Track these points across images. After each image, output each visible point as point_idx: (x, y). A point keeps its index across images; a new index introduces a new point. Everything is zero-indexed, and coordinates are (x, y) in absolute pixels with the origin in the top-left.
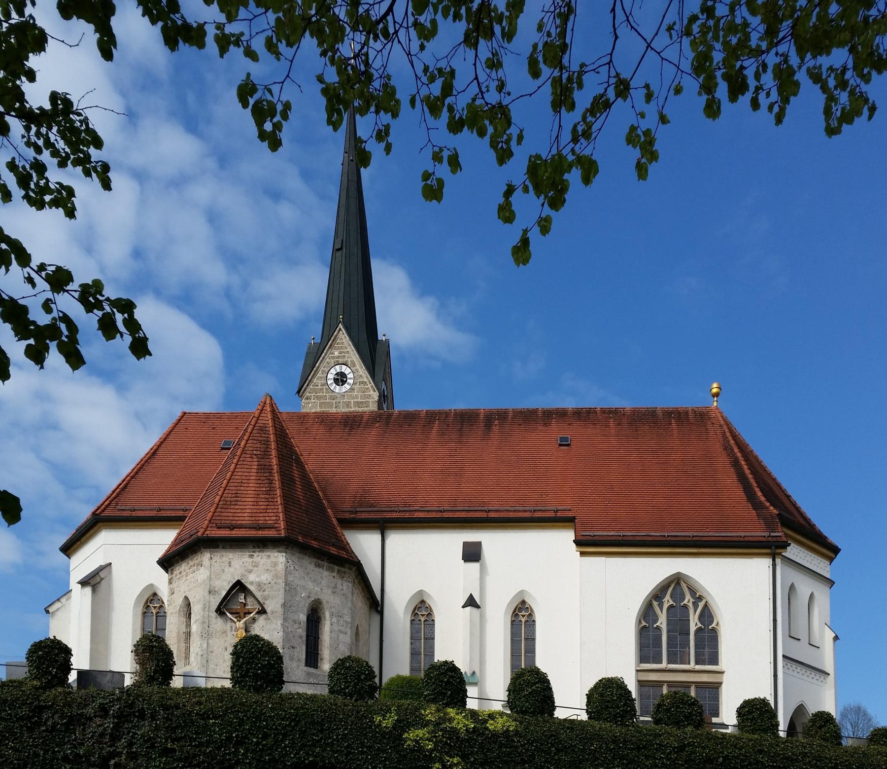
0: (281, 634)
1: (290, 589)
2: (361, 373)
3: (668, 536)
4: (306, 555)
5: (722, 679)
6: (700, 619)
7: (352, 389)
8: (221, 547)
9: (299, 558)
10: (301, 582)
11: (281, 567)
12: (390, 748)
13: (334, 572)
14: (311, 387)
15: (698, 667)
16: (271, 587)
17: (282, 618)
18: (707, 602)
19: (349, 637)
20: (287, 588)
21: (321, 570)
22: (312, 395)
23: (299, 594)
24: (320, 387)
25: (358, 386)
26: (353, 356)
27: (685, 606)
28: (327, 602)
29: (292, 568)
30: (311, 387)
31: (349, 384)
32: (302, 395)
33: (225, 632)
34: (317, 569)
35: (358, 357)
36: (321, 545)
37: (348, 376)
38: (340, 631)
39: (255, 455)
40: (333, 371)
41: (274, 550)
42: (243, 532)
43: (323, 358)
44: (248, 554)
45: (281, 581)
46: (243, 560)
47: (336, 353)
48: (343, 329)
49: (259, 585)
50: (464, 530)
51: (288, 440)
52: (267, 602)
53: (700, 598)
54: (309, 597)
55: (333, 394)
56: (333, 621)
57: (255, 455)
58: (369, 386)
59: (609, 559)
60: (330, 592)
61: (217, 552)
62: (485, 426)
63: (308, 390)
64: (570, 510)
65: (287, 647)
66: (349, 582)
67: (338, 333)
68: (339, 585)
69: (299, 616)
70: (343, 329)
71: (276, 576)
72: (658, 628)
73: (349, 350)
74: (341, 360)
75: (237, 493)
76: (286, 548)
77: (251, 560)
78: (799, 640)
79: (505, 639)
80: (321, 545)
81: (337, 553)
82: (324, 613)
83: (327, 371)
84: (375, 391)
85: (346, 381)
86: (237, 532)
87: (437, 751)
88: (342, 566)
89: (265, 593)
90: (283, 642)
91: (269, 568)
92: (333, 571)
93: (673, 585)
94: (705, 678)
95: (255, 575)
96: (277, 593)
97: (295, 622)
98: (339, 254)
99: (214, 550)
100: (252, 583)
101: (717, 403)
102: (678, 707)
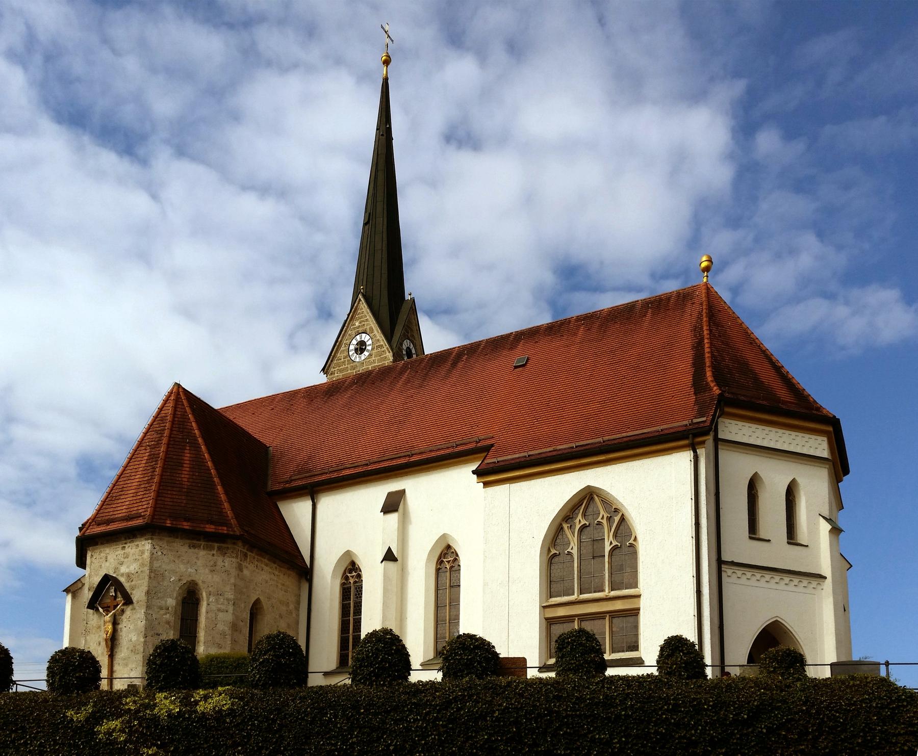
0: (144, 622)
1: (155, 575)
2: (378, 338)
3: (576, 447)
4: (177, 538)
5: (639, 604)
6: (615, 536)
7: (370, 355)
8: (99, 543)
9: (168, 542)
10: (172, 566)
11: (147, 555)
12: (82, 743)
13: (214, 550)
14: (335, 362)
15: (614, 593)
16: (138, 577)
17: (145, 607)
18: (623, 514)
19: (231, 615)
20: (153, 575)
21: (196, 550)
22: (336, 369)
23: (168, 579)
24: (342, 360)
25: (376, 351)
26: (372, 323)
27: (599, 524)
28: (203, 582)
29: (160, 553)
30: (335, 362)
31: (368, 351)
32: (327, 372)
33: (99, 627)
34: (192, 550)
35: (375, 322)
36: (195, 525)
37: (367, 343)
38: (219, 610)
39: (149, 446)
40: (354, 342)
41: (142, 539)
42: (116, 526)
43: (346, 331)
44: (121, 546)
45: (146, 569)
46: (117, 553)
47: (357, 324)
48: (362, 299)
49: (129, 576)
50: (372, 483)
51: (189, 424)
52: (134, 592)
53: (616, 511)
54: (180, 580)
55: (355, 364)
56: (211, 600)
57: (149, 446)
58: (385, 348)
59: (513, 485)
60: (207, 571)
61: (97, 549)
62: (452, 364)
63: (333, 365)
64: (493, 437)
65: (150, 634)
66: (233, 557)
67: (359, 303)
68: (220, 563)
69: (166, 601)
70: (362, 299)
71: (143, 565)
72: (569, 553)
73: (368, 317)
74: (361, 330)
75: (123, 488)
76: (152, 535)
77: (123, 552)
78: (769, 541)
79: (427, 591)
80: (195, 525)
81: (213, 530)
82: (202, 594)
83: (349, 343)
84: (389, 352)
85: (365, 348)
86: (112, 527)
87: (131, 743)
88: (224, 542)
89: (133, 583)
90: (145, 630)
91: (137, 557)
92: (212, 548)
93: (585, 503)
94: (619, 605)
95: (125, 567)
96: (143, 581)
97: (161, 608)
98: (367, 227)
99: (95, 547)
100: (122, 575)
101: (707, 279)
102: (456, 654)
